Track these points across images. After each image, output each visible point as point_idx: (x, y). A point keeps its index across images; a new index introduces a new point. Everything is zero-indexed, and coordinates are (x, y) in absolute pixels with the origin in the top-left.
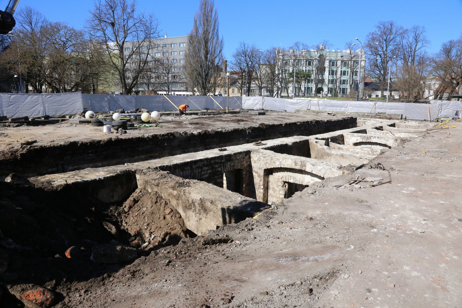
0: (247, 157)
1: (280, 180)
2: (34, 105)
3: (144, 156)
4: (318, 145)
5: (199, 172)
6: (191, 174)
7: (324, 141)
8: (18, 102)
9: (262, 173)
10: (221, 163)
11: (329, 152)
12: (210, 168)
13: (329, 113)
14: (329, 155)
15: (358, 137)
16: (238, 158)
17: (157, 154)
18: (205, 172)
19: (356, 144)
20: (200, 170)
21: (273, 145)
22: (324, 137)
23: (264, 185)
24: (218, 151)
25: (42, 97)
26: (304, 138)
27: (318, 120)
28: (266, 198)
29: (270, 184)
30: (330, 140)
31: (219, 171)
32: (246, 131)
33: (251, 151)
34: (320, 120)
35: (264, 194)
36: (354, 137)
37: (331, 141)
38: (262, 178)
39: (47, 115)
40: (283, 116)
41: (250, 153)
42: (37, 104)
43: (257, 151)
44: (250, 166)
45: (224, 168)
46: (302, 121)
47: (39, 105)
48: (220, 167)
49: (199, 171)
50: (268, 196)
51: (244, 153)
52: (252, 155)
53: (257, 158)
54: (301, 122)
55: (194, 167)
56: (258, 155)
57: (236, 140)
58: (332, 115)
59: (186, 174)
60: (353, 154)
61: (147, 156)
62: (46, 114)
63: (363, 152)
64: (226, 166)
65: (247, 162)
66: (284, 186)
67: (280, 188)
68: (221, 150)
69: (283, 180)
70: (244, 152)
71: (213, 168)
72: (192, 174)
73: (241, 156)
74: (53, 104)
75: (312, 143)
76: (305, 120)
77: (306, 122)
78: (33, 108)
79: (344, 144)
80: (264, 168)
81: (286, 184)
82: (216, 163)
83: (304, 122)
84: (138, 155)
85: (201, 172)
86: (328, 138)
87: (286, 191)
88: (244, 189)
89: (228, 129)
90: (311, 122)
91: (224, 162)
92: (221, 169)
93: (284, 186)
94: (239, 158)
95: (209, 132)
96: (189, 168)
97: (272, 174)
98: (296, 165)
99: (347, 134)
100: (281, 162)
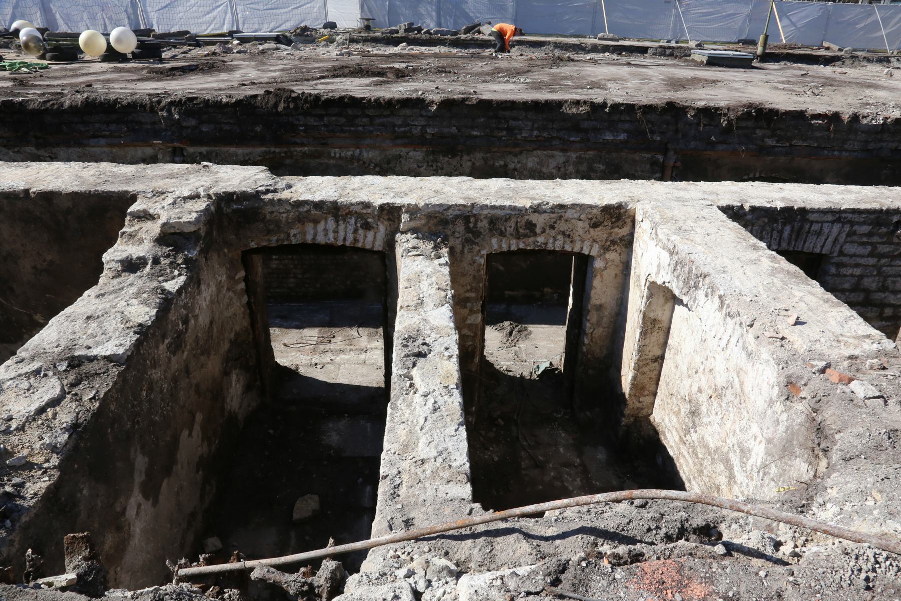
2: (211, 8)
57: (103, 141)
78: (208, 13)
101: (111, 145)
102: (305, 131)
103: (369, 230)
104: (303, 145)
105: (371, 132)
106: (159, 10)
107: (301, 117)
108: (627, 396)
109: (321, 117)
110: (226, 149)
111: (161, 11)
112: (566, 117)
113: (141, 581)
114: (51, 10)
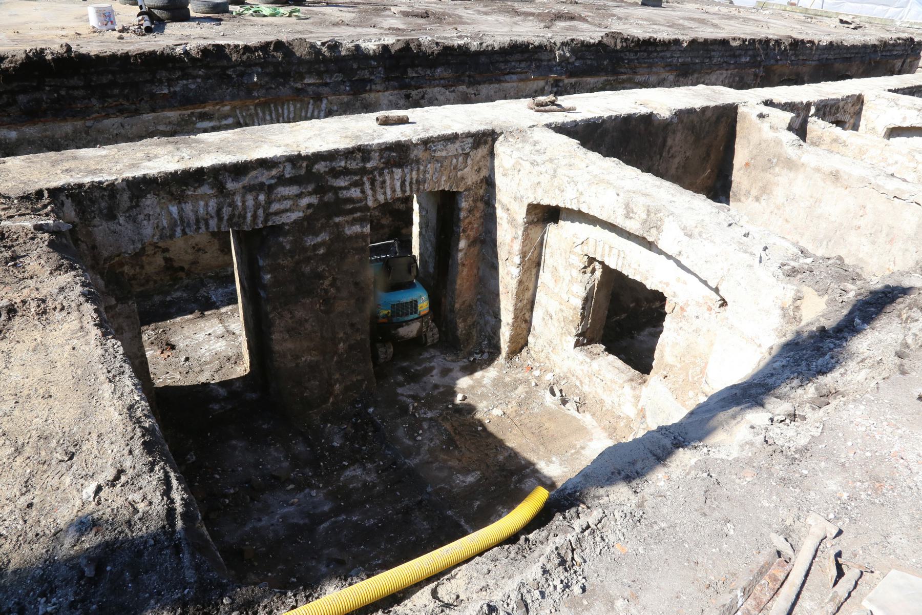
0: (483, 151)
1: (578, 250)
3: (179, 112)
4: (765, 125)
5: (257, 206)
6: (219, 212)
7: (787, 117)
9: (521, 215)
10: (363, 171)
11: (794, 157)
12: (310, 188)
13: (845, 19)
14: (790, 164)
15: (909, 108)
16: (438, 154)
17: (227, 108)
18: (287, 204)
19: (894, 132)
20: (262, 197)
21: (597, 115)
22: (797, 100)
23: (523, 255)
24: (375, 125)
26: (721, 95)
27: (800, 37)
28: (530, 292)
29: (547, 253)
30: (813, 110)
31: (350, 200)
32: (552, 51)
33: (498, 131)
34: (807, 38)
35: (520, 282)
36: (896, 108)
37: (815, 115)
38: (520, 233)
40: (704, 16)
41: (494, 140)
43: (520, 133)
44: (489, 183)
45: (373, 188)
46: (748, 38)
48: (359, 184)
49: (256, 199)
50: (536, 288)
51: (470, 140)
52: (500, 147)
53: (512, 161)
54: (744, 41)
55: (230, 185)
56: (518, 149)
57: (514, 77)
58: (852, 26)
59: (196, 212)
60: (875, 177)
61: (189, 112)
63: (913, 165)
64: (384, 182)
65: (479, 170)
66: (589, 269)
67: (576, 274)
68: (386, 122)
69: (586, 252)
70: (469, 135)
71: (320, 190)
72: (226, 211)
73: (453, 148)
75: (745, 116)
76: (761, 33)
77: (760, 41)
79: (855, 127)
80: (530, 201)
81: (598, 266)
82: (335, 173)
83: (752, 42)
84: (153, 110)
85: (269, 202)
86: (808, 105)
87: (592, 288)
88: (460, 255)
89: (490, 42)
90: (778, 42)
91: (375, 168)
92: (363, 192)
93: (589, 269)
94: (444, 154)
95: (419, 45)
96: (210, 192)
97: (557, 223)
98: (627, 216)
99: (878, 97)
100: (581, 194)
101: (521, 80)
102: (628, 63)
104: (625, 74)
105: (657, 62)
107: (627, 53)
109: (636, 52)
110: (584, 79)
112: (732, 48)
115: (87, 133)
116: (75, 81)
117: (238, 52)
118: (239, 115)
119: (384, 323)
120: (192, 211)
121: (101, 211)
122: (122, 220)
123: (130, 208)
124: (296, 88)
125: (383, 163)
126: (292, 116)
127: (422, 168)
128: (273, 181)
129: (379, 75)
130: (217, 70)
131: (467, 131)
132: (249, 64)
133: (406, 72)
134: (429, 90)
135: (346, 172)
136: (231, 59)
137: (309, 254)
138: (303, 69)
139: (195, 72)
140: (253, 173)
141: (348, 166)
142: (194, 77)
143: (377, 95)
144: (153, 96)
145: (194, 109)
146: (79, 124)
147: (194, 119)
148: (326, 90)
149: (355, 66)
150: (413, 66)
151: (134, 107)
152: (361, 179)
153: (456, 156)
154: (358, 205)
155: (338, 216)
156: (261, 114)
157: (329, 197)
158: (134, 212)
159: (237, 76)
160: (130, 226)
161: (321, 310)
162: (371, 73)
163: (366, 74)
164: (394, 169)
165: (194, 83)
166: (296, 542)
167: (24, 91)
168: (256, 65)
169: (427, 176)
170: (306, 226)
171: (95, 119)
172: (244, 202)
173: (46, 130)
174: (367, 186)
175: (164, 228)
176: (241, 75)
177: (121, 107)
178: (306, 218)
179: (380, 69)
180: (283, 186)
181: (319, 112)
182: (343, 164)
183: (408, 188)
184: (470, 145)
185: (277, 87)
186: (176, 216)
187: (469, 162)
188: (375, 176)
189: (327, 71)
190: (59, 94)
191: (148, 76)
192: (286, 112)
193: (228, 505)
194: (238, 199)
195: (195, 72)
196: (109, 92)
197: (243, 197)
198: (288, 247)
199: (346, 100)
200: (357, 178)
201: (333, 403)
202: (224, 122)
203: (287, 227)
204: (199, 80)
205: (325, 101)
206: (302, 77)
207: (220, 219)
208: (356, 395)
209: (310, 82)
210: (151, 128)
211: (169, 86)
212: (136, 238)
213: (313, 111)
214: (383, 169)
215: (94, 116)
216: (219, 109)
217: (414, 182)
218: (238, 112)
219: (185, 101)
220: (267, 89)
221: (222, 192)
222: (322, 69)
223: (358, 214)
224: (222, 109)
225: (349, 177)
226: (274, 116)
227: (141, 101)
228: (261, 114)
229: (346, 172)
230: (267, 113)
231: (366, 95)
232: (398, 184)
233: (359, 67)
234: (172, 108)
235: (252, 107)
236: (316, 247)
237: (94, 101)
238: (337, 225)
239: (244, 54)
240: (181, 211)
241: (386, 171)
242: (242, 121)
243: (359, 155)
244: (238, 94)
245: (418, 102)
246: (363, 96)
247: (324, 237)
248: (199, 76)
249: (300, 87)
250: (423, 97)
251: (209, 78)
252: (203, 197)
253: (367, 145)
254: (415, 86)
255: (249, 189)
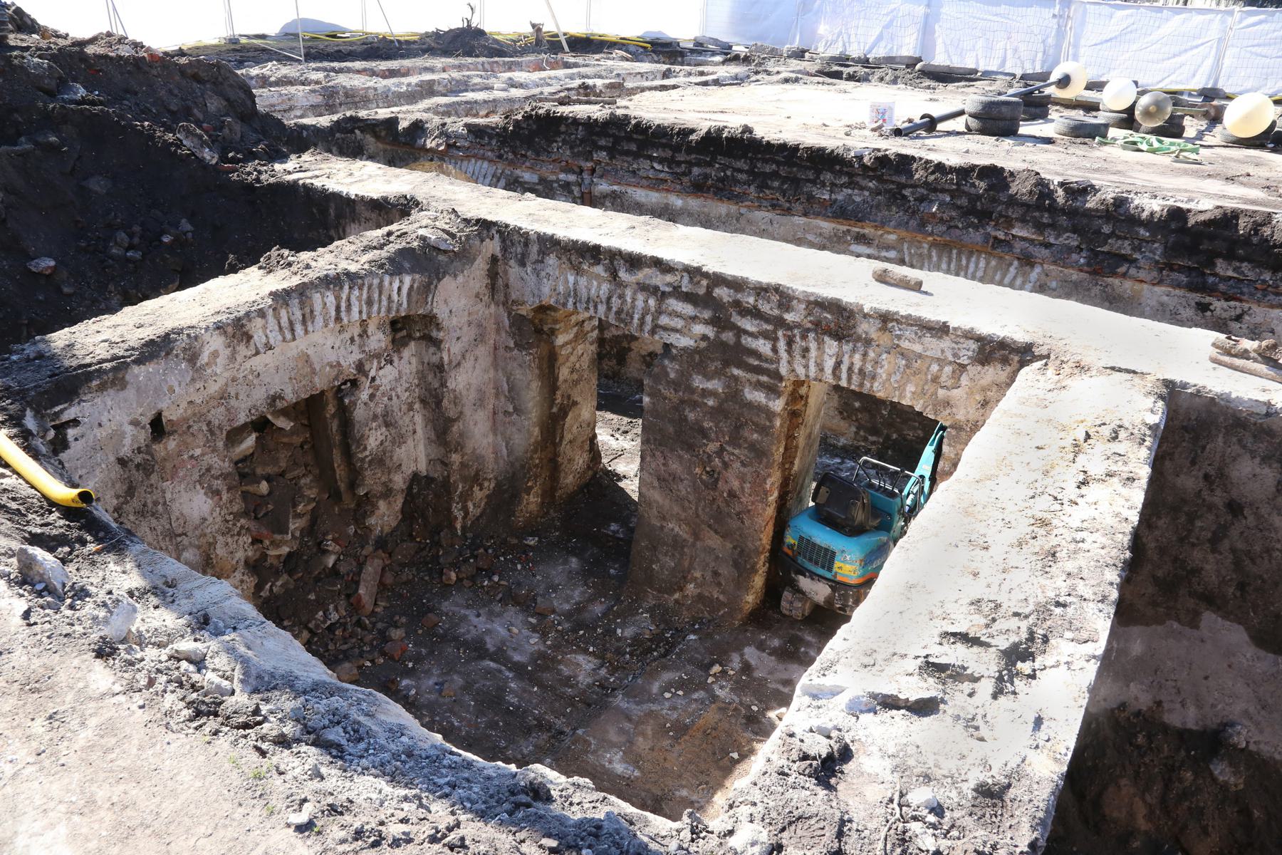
0: (993, 373)
2: (1183, 48)
3: (833, 225)
5: (646, 311)
8: (1131, 32)
10: (780, 323)
16: (905, 344)
17: (893, 237)
25: (1223, 22)
31: (755, 354)
39: (1220, 86)
41: (1023, 364)
42: (1195, 43)
45: (789, 351)
47: (1202, 47)
61: (845, 228)
62: (1216, 81)
64: (807, 350)
68: (882, 278)
70: (969, 335)
71: (720, 322)
72: (616, 302)
73: (933, 346)
74: (1254, 49)
78: (1175, 56)
84: (805, 215)
85: (659, 312)
91: (798, 325)
92: (775, 350)
94: (917, 348)
96: (603, 274)
103: (582, 276)
106: (1096, 45)
108: (631, 487)
111: (1099, 47)
113: (367, 622)
114: (934, 32)
115: (738, 220)
116: (740, 164)
117: (926, 169)
118: (905, 250)
119: (787, 555)
120: (586, 287)
121: (516, 255)
122: (529, 269)
123: (537, 261)
124: (995, 238)
125: (810, 322)
126: (979, 274)
127: (872, 354)
128: (668, 289)
129: (1151, 255)
130: (892, 186)
131: (967, 327)
132: (933, 188)
133: (1212, 265)
134: (1255, 308)
135: (756, 313)
136: (912, 176)
137: (696, 397)
138: (1014, 213)
139: (864, 182)
140: (647, 271)
141: (760, 307)
142: (862, 188)
143: (1137, 286)
144: (810, 198)
145: (863, 227)
146: (733, 208)
147: (849, 238)
148: (1045, 252)
149: (1106, 229)
150: (1230, 256)
151: (788, 205)
152: (775, 332)
153: (941, 362)
154: (765, 365)
155: (738, 367)
156: (935, 259)
157: (728, 336)
158: (539, 266)
159: (915, 200)
160: (534, 278)
161: (701, 479)
162: (1136, 249)
163: (1126, 248)
164: (826, 339)
165: (860, 195)
166: (458, 649)
167: (698, 164)
168: (943, 191)
169: (879, 371)
170: (696, 359)
171: (748, 207)
172: (634, 300)
173: (705, 206)
174: (782, 345)
175: (559, 293)
176: (921, 199)
177: (775, 202)
178: (696, 351)
179: (1156, 245)
180: (677, 298)
181: (1024, 283)
182: (751, 300)
183: (844, 376)
184: (970, 353)
185: (966, 228)
186: (571, 285)
187: (964, 380)
188: (795, 336)
189: (1053, 226)
190: (725, 174)
191: (811, 175)
192: (972, 266)
193: (483, 587)
194: (629, 293)
195: (864, 182)
196: (769, 182)
197: (635, 293)
198: (672, 375)
199: (1074, 277)
200: (770, 327)
201: (677, 601)
202: (884, 254)
203: (674, 351)
204: (867, 193)
205: (1038, 270)
206: (1009, 224)
207: (609, 308)
208: (706, 614)
209: (1020, 234)
210: (800, 235)
211: (832, 192)
212: (536, 292)
213: (1015, 278)
214: (808, 330)
215: (747, 203)
216: (882, 235)
217: (856, 371)
218: (906, 246)
219: (841, 213)
220: (949, 227)
221: (615, 280)
222: (1045, 221)
223: (764, 379)
224: (886, 236)
225: (758, 322)
226: (953, 266)
227: (797, 200)
228: (935, 259)
229: (756, 313)
230: (945, 259)
231: (1116, 282)
232: (829, 364)
233: (1113, 233)
234: (826, 217)
235: (926, 246)
236: (706, 393)
237: (752, 189)
238: (736, 379)
239: (933, 173)
240: (576, 283)
241: (811, 335)
242: (907, 259)
243: (775, 298)
244: (907, 223)
245: (1225, 324)
246: (1110, 280)
247: (715, 385)
248: (869, 189)
249: (1003, 238)
250: (1238, 318)
251: (879, 194)
252: (597, 277)
253: (788, 288)
254: (1224, 293)
255: (643, 287)
